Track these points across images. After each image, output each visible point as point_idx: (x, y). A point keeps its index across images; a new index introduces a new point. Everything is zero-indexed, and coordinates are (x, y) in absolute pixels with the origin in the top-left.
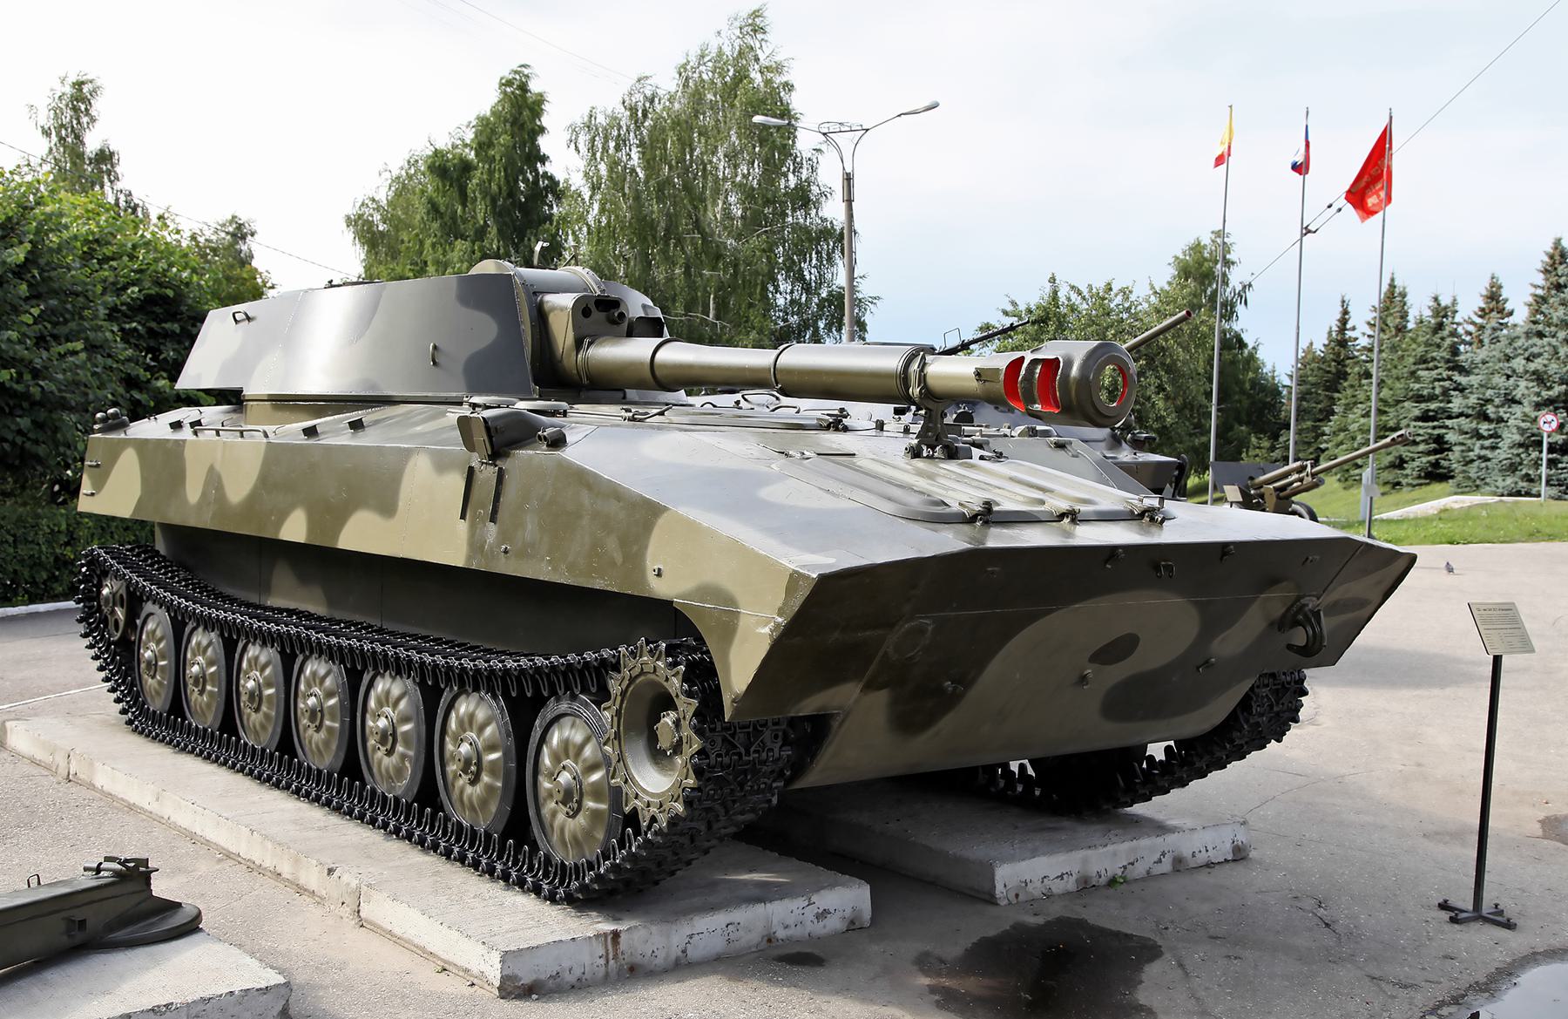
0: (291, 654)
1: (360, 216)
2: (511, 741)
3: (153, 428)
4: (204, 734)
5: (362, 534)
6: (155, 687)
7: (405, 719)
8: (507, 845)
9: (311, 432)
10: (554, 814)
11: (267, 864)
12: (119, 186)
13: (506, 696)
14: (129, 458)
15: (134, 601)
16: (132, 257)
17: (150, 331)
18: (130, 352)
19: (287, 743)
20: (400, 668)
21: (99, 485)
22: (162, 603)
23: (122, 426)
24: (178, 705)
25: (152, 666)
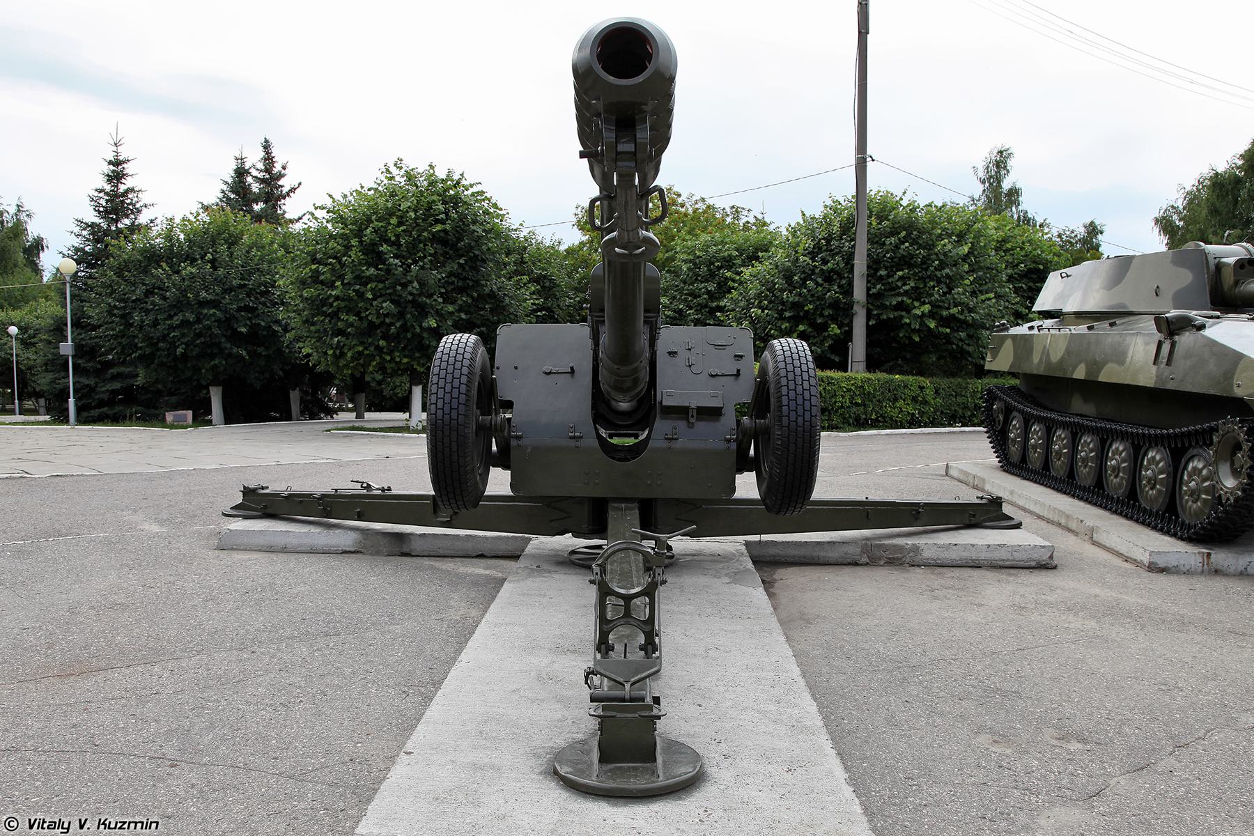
0: (1076, 432)
1: (1164, 218)
3: (1022, 329)
4: (1035, 472)
6: (1014, 449)
7: (1124, 461)
8: (1165, 518)
11: (1056, 519)
12: (1020, 208)
13: (1169, 447)
14: (1009, 343)
15: (1008, 411)
16: (1022, 249)
17: (1030, 288)
18: (1018, 299)
19: (1071, 474)
21: (994, 357)
22: (1019, 411)
23: (1007, 329)
24: (1024, 459)
25: (1014, 441)
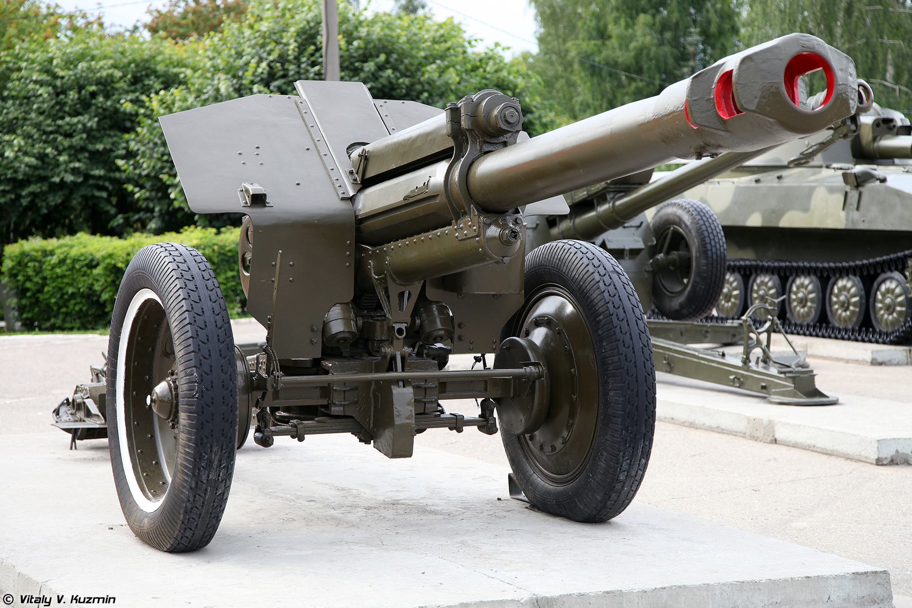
2: (742, 286)
5: (792, 220)
9: (757, 181)
10: (796, 307)
20: (806, 272)
